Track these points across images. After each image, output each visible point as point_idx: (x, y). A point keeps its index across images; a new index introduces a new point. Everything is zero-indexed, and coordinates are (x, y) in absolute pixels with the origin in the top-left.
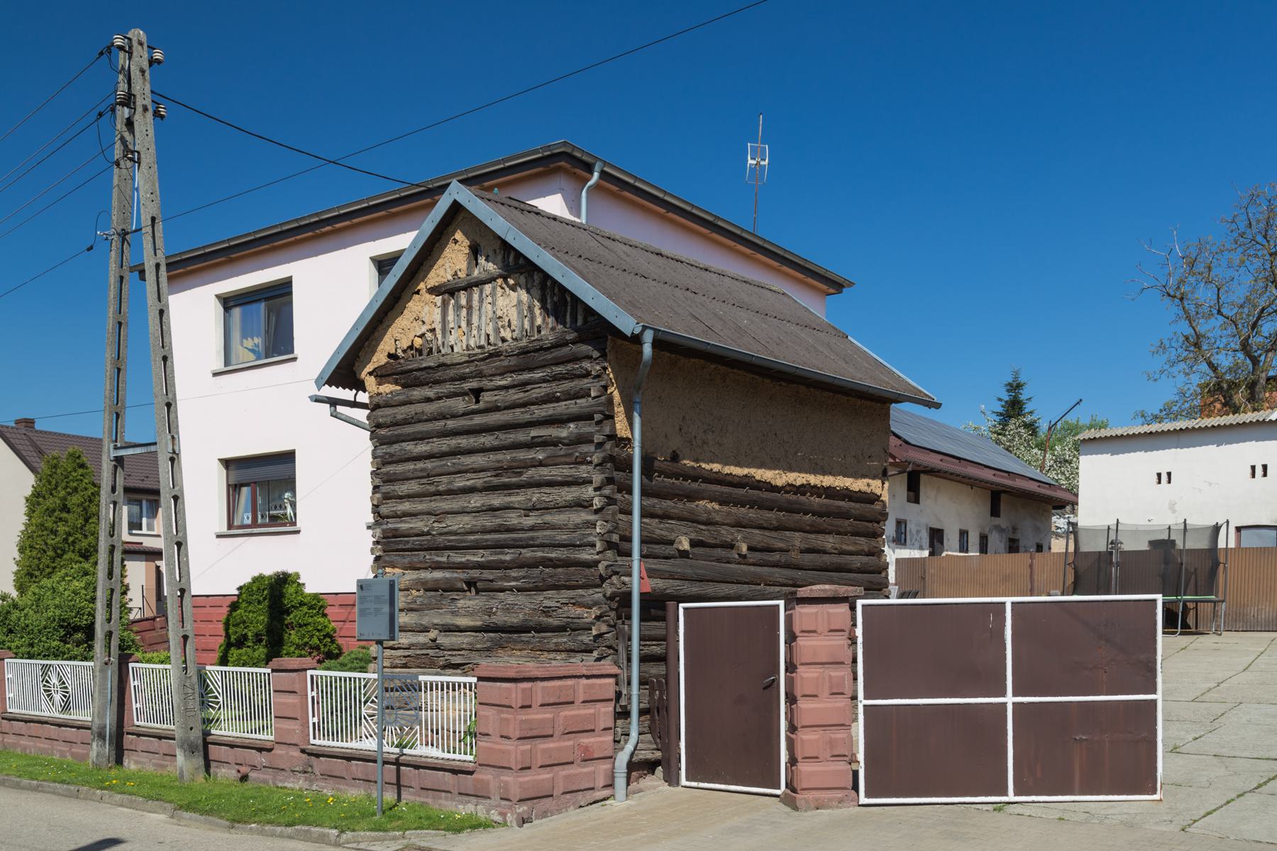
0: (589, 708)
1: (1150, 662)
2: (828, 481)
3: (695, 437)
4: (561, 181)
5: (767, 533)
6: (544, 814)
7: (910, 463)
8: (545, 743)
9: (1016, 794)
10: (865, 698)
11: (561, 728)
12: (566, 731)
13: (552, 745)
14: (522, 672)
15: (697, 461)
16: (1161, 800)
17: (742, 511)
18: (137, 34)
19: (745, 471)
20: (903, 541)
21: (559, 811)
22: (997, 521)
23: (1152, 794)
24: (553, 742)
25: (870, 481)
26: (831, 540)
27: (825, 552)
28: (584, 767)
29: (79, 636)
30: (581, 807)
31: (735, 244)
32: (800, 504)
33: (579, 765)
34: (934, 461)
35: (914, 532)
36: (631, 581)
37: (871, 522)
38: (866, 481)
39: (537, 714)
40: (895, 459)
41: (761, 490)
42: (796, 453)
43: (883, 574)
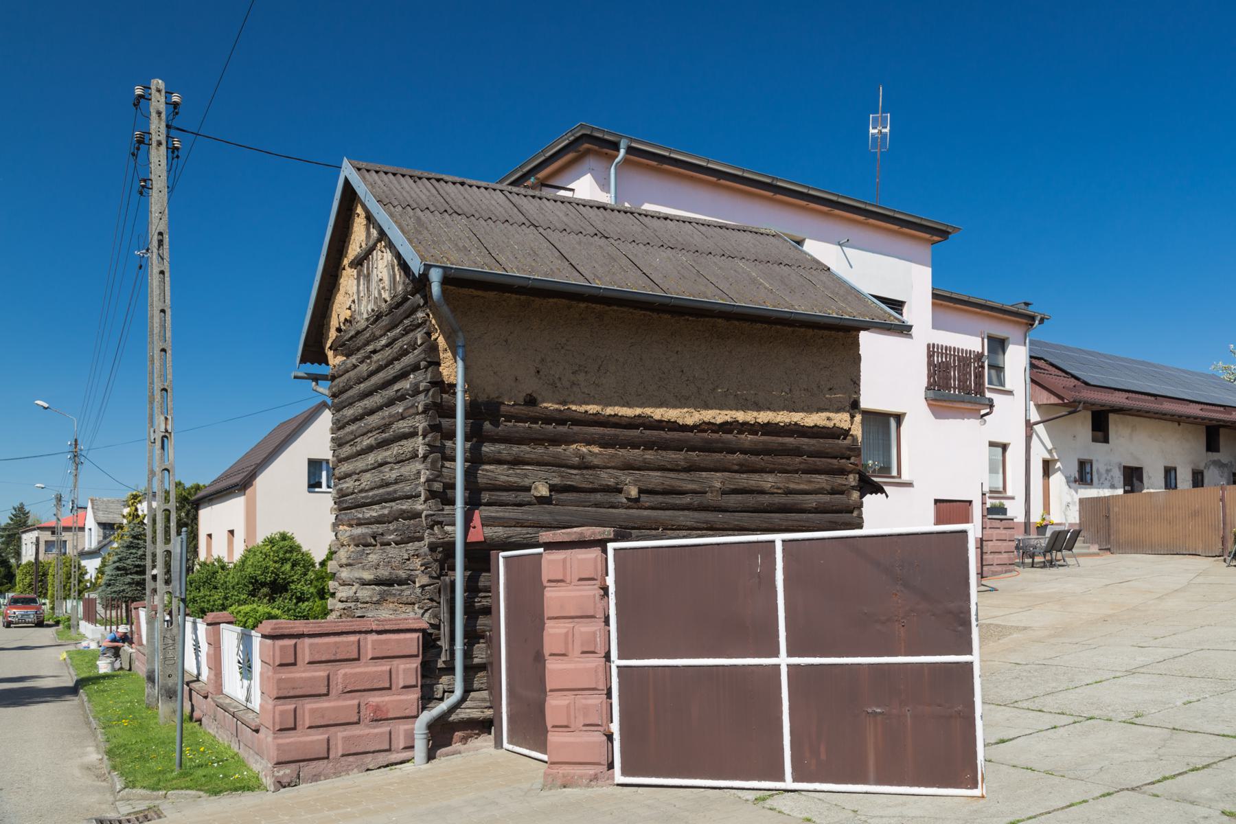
0: (383, 665)
1: (962, 612)
2: (764, 417)
3: (560, 379)
4: (591, 162)
5: (672, 475)
6: (315, 778)
7: (1080, 402)
9: (795, 780)
10: (620, 657)
11: (340, 687)
12: (346, 690)
13: (326, 705)
14: (282, 628)
15: (564, 403)
16: (983, 797)
17: (693, 455)
18: (157, 83)
19: (638, 411)
20: (1173, 485)
21: (337, 774)
22: (1215, 456)
23: (971, 788)
24: (330, 701)
25: (831, 415)
26: (770, 480)
28: (375, 728)
29: (265, 590)
30: (368, 770)
32: (722, 443)
33: (367, 726)
34: (1119, 399)
35: (1102, 470)
36: (454, 531)
37: (835, 458)
39: (304, 672)
40: (1063, 401)
41: (664, 430)
43: (855, 514)
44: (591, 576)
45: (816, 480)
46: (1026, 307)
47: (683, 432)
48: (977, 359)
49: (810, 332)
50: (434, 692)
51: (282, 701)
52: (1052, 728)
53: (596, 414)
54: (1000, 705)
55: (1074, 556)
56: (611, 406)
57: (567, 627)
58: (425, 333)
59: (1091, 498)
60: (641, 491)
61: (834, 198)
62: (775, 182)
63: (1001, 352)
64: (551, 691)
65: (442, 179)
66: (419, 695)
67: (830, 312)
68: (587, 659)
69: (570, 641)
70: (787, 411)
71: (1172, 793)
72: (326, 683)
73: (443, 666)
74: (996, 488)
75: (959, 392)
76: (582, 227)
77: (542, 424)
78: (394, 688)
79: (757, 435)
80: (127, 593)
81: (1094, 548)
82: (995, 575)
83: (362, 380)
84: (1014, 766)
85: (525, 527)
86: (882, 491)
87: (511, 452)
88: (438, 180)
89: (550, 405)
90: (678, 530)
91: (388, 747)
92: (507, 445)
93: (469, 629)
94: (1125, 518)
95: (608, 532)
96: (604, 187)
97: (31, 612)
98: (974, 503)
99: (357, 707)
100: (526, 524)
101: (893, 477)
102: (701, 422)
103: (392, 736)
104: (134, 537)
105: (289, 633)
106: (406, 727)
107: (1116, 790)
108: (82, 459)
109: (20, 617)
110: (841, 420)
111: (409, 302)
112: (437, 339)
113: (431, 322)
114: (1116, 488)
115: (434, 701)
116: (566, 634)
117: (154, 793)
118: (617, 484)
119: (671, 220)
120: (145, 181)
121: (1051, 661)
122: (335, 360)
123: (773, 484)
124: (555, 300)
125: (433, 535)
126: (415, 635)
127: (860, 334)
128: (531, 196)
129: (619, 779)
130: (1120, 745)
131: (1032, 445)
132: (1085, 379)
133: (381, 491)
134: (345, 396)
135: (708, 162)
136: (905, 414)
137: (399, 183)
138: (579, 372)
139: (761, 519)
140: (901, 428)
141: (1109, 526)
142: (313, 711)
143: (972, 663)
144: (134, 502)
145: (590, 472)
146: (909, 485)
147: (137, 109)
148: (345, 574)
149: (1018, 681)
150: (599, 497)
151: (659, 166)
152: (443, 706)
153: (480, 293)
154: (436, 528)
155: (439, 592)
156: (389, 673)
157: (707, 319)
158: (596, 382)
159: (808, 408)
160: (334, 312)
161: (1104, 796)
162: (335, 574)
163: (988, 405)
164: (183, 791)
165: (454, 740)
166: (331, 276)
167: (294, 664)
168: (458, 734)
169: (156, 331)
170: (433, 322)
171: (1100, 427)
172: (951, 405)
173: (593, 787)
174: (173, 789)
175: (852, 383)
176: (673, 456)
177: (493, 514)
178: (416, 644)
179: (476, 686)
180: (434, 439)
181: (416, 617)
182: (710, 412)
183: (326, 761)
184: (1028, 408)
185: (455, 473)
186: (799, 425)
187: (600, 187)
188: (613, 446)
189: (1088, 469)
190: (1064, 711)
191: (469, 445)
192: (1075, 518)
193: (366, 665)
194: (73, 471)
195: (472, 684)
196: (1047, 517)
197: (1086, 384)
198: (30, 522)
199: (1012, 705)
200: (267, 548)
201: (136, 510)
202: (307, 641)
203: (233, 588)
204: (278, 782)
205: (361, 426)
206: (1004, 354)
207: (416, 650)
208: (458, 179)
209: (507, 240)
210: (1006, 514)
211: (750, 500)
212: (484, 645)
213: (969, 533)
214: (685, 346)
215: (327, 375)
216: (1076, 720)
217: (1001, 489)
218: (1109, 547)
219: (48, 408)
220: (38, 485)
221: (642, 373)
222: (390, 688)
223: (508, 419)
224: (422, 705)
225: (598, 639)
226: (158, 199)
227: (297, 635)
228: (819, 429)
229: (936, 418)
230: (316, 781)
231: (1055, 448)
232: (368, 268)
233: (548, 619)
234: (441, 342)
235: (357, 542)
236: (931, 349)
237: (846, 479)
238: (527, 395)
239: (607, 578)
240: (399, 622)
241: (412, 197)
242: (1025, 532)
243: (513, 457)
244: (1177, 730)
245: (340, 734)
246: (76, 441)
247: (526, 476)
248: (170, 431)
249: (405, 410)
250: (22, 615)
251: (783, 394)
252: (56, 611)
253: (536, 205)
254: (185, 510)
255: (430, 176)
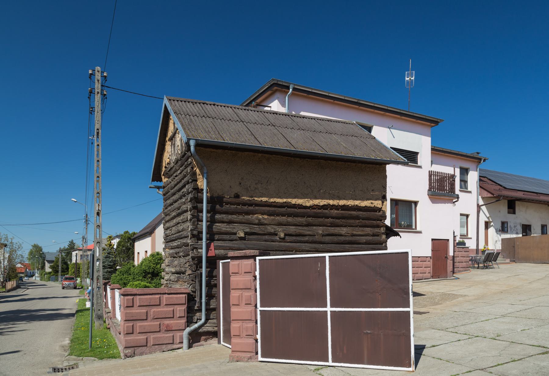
2: (342, 202)
3: (250, 187)
4: (278, 95)
5: (300, 228)
6: (141, 354)
7: (501, 196)
8: (141, 323)
9: (333, 362)
10: (261, 307)
11: (152, 316)
14: (127, 292)
15: (252, 197)
16: (413, 371)
17: (310, 219)
18: (98, 68)
19: (285, 200)
20: (545, 233)
21: (150, 353)
23: (408, 367)
24: (147, 322)
27: (341, 235)
28: (167, 334)
29: (149, 275)
30: (164, 351)
31: (374, 110)
33: (163, 333)
34: (520, 195)
35: (512, 226)
38: (370, 201)
39: (137, 310)
40: (494, 195)
41: (296, 208)
42: (319, 191)
43: (384, 245)
44: (250, 271)
45: (365, 230)
46: (477, 155)
47: (305, 209)
48: (452, 177)
49: (364, 165)
50: (193, 319)
51: (127, 322)
52: (458, 341)
53: (266, 202)
54: (440, 330)
55: (497, 264)
56: (272, 198)
57: (239, 293)
58: (191, 168)
59: (507, 238)
60: (285, 235)
61: (386, 108)
62: (359, 101)
63: (466, 174)
64: (233, 320)
65: (205, 103)
66: (186, 320)
67: (372, 156)
68: (247, 307)
69: (241, 299)
70: (353, 200)
71: (499, 372)
72: (146, 315)
73: (197, 308)
74: (463, 234)
75: (438, 191)
76: (264, 122)
77: (242, 206)
78: (175, 317)
79: (339, 210)
80: (105, 276)
81: (508, 261)
82: (460, 272)
83: (172, 188)
84: (433, 358)
85: (233, 250)
86: (399, 235)
87: (228, 218)
88: (204, 104)
89: (245, 198)
90: (302, 251)
91: (172, 342)
92: (226, 215)
93: (209, 293)
94: (522, 247)
95: (256, 252)
96: (283, 105)
97: (72, 283)
98: (450, 240)
99: (159, 325)
100: (234, 249)
101: (413, 229)
102: (313, 205)
103: (174, 338)
104: (108, 254)
105: (130, 294)
106: (181, 334)
107: (474, 370)
108: (89, 222)
109: (68, 285)
110: (377, 204)
111: (186, 155)
112: (196, 170)
113: (193, 163)
114: (519, 234)
115: (193, 323)
116: (239, 296)
117: (78, 358)
118: (275, 232)
119: (306, 118)
120: (92, 108)
121: (470, 310)
122: (165, 180)
123: (346, 232)
124: (248, 153)
125: (193, 253)
126: (184, 295)
127: (387, 166)
128: (244, 109)
129: (260, 359)
130: (484, 349)
131: (480, 215)
132: (504, 186)
133: (178, 234)
134: (167, 195)
135: (329, 93)
136: (418, 201)
137: (186, 105)
138: (258, 184)
139: (340, 247)
140: (417, 208)
141: (515, 250)
142: (140, 326)
143: (410, 311)
144: (110, 239)
145: (263, 226)
146: (420, 232)
147: (90, 79)
148: (167, 269)
149: (453, 319)
150: (267, 237)
151: (308, 96)
152: (196, 326)
153: (215, 150)
154: (194, 250)
155: (196, 277)
156: (173, 311)
157: (316, 160)
158: (266, 188)
159: (363, 199)
160: (164, 160)
161: (467, 372)
162: (164, 269)
163: (456, 197)
164: (89, 358)
165: (201, 340)
166: (162, 145)
167: (133, 306)
168: (203, 338)
169: (95, 169)
170: (194, 163)
171: (512, 206)
172: (439, 197)
173: (249, 362)
174: (85, 357)
175: (383, 187)
176: (300, 220)
177: (219, 244)
178: (184, 299)
179: (211, 317)
180: (194, 213)
181: (186, 288)
182: (317, 200)
183: (146, 347)
184: (478, 199)
185: (203, 227)
186: (358, 206)
187: (282, 106)
188: (273, 215)
189: (506, 226)
190: (466, 333)
191: (209, 215)
192: (499, 247)
193: (163, 307)
194: (85, 227)
195: (210, 317)
196: (487, 247)
197: (505, 188)
198: (75, 247)
199: (445, 330)
200: (151, 258)
201: (111, 242)
202: (138, 297)
203: (137, 274)
204: (125, 355)
205: (172, 208)
206: (467, 175)
207: (185, 302)
208: (212, 103)
209: (228, 128)
210: (465, 245)
211: (335, 239)
212: (215, 300)
213: (409, 253)
214: (306, 172)
215: (162, 186)
216: (470, 337)
217: (466, 235)
218: (514, 260)
219: (76, 201)
220: (75, 232)
221: (287, 184)
222: (173, 317)
223: (227, 204)
224: (187, 325)
225: (252, 299)
226: (97, 116)
227: (134, 294)
228: (368, 208)
229: (433, 203)
230: (142, 355)
231: (490, 216)
232: (174, 141)
234: (198, 171)
235: (171, 256)
236: (431, 173)
237: (380, 229)
238: (235, 193)
239: (256, 272)
240: (177, 290)
241: (190, 111)
242: (476, 253)
243: (229, 220)
244: (513, 342)
245: (152, 336)
246: (87, 215)
247: (234, 228)
248: (100, 210)
249: (185, 200)
250: (69, 284)
251: (351, 192)
252: (82, 283)
253: (246, 113)
254: (129, 243)
255: (201, 102)
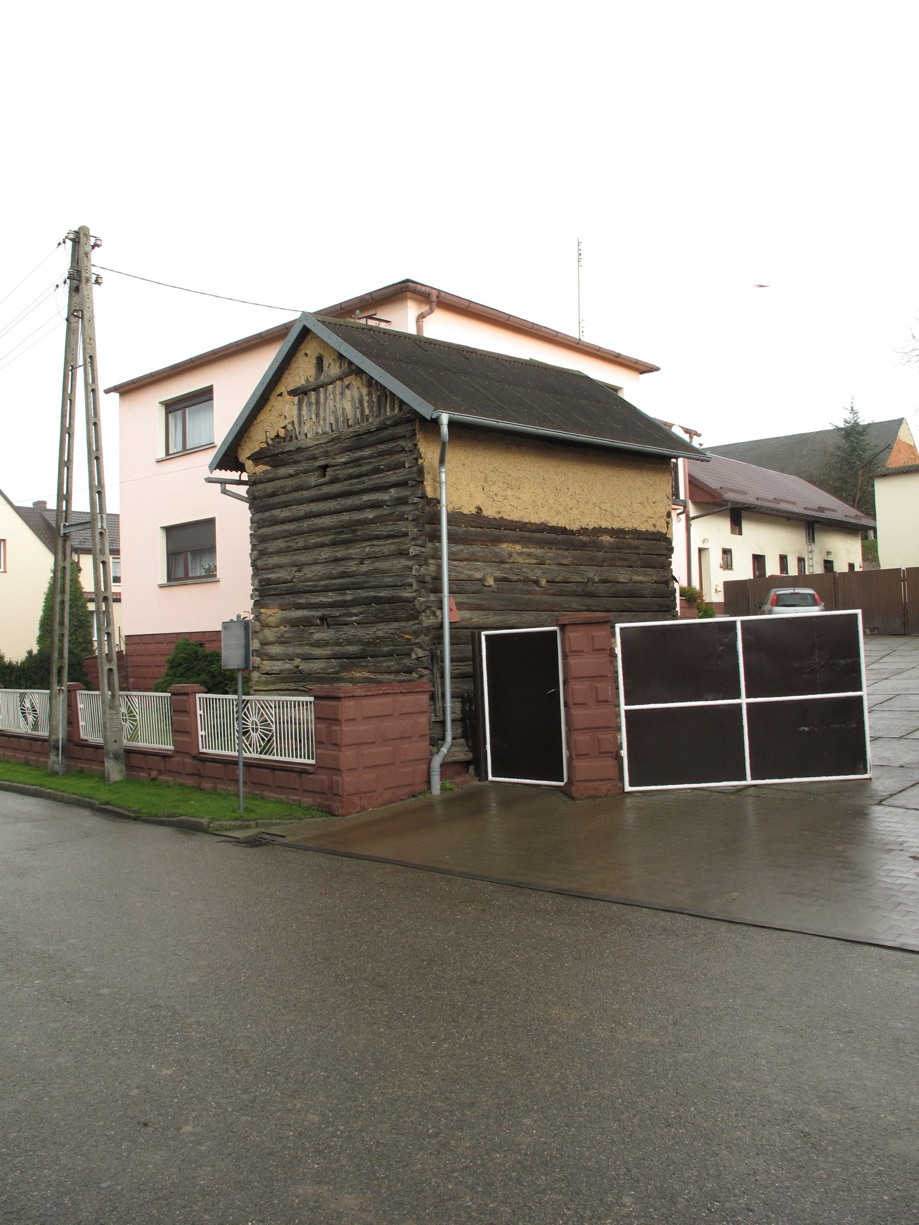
10: (626, 704)
45: (649, 572)
233: (571, 679)
